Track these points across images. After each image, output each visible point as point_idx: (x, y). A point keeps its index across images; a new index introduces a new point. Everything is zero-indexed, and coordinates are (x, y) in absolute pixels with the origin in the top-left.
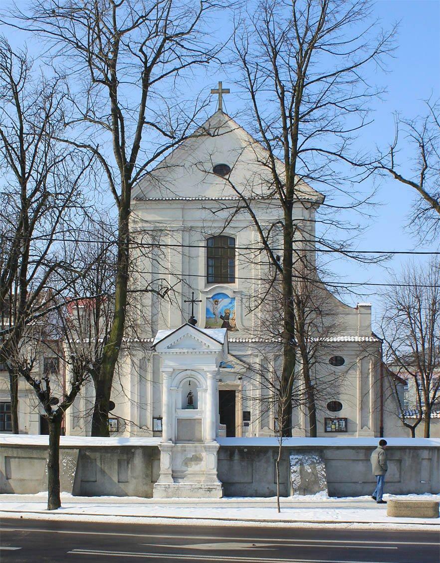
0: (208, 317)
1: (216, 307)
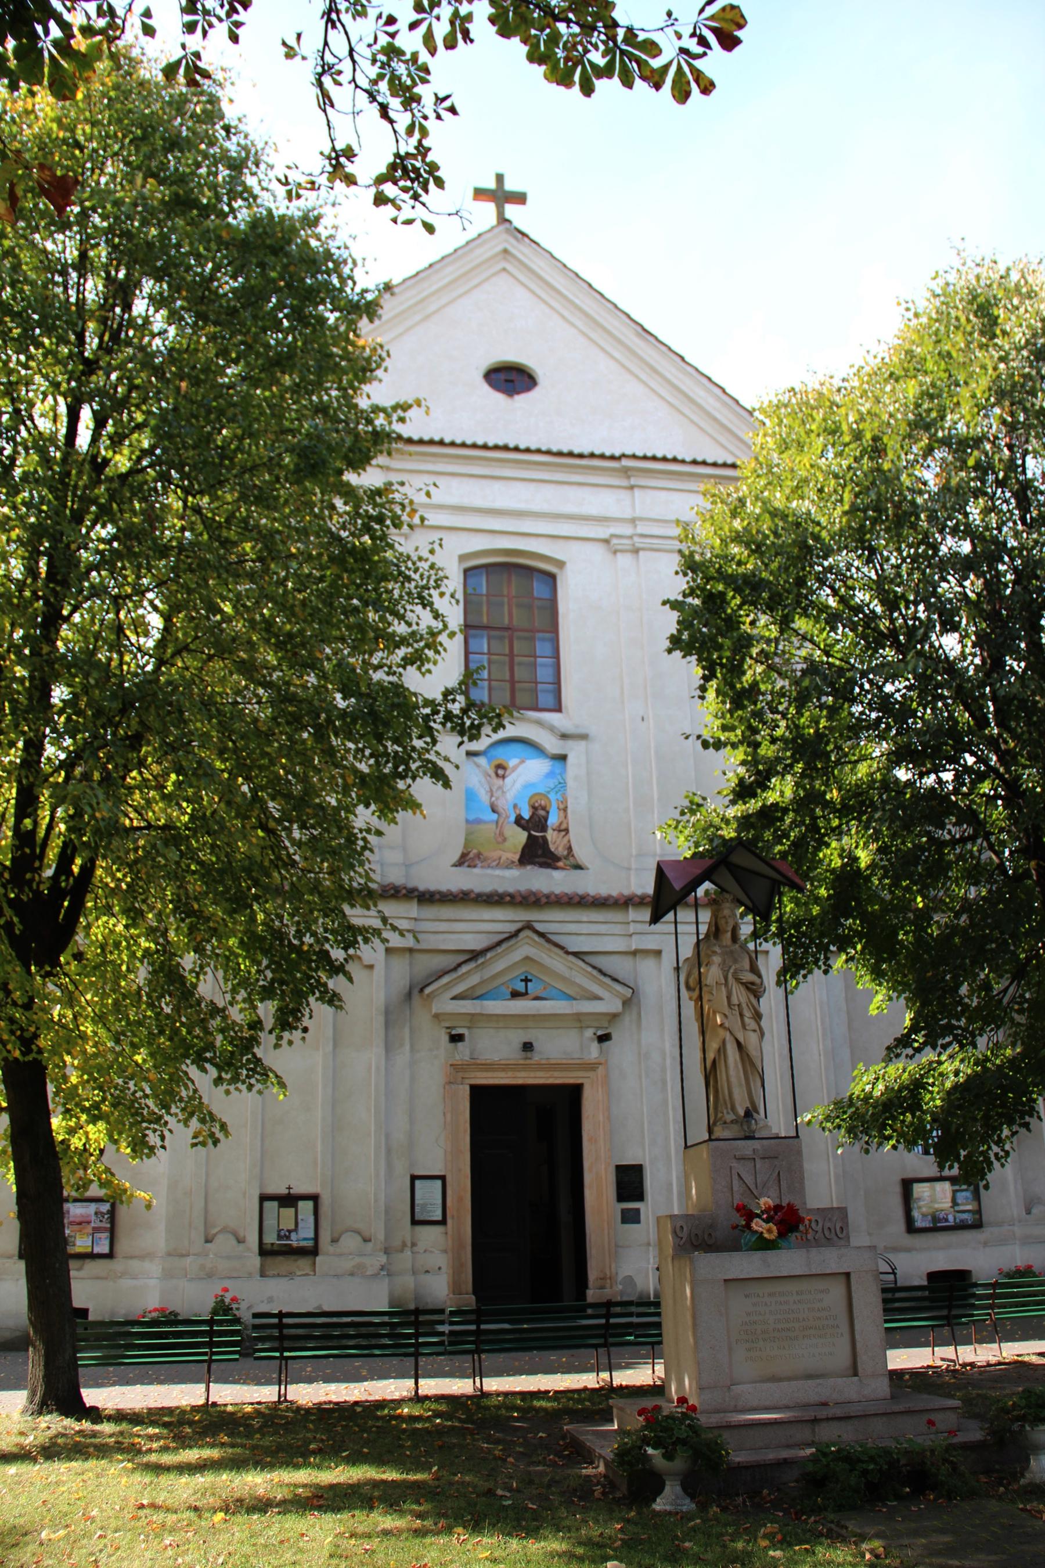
0: (471, 817)
1: (500, 788)
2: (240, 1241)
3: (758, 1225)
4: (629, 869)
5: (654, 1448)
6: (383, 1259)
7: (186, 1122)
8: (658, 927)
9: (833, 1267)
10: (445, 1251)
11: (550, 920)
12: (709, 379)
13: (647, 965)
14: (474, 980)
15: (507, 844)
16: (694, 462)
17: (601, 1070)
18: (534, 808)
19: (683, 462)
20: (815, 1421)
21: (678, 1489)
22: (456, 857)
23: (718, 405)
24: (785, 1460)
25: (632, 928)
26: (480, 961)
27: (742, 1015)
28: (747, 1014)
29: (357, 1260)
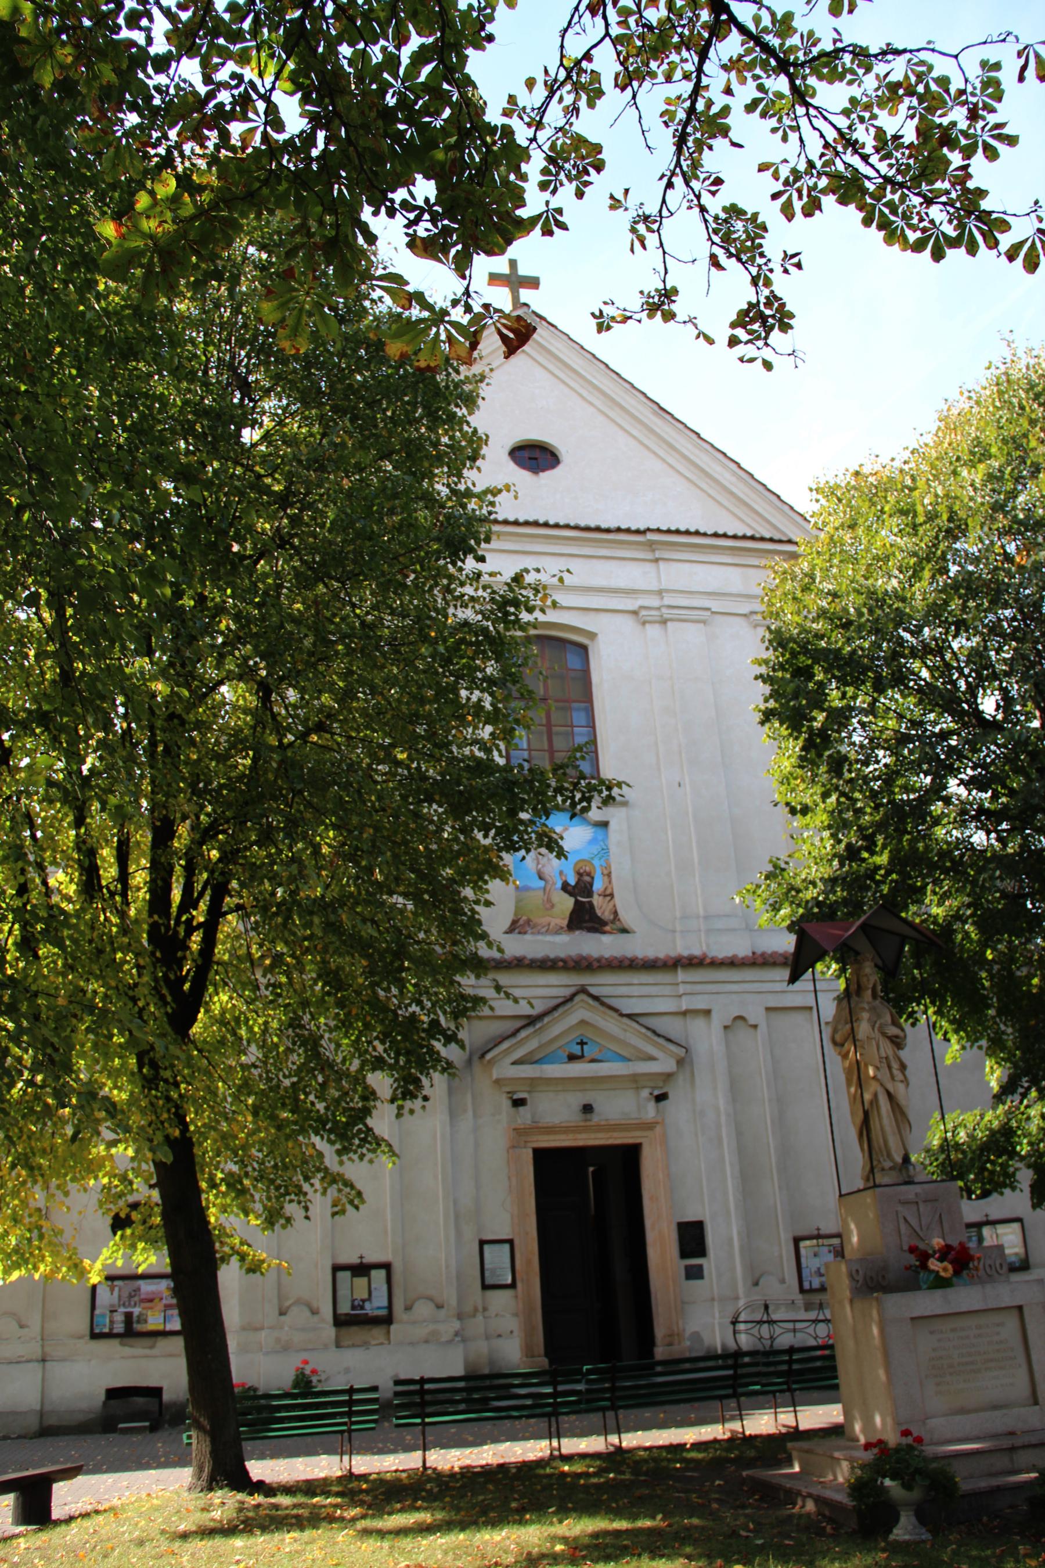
2: (314, 1312)
3: (934, 1264)
4: (674, 931)
5: (892, 1479)
6: (457, 1325)
7: (324, 1192)
8: (798, 985)
9: (1007, 1301)
10: (516, 1315)
11: (604, 984)
12: (725, 454)
13: (697, 1025)
14: (533, 1044)
15: (555, 910)
16: (716, 535)
17: (658, 1129)
18: (580, 874)
19: (705, 535)
20: (1013, 1449)
21: (913, 1519)
22: (507, 924)
23: (734, 479)
24: (998, 1487)
25: (682, 989)
26: (538, 1026)
27: (890, 1067)
28: (895, 1066)
29: (432, 1327)
